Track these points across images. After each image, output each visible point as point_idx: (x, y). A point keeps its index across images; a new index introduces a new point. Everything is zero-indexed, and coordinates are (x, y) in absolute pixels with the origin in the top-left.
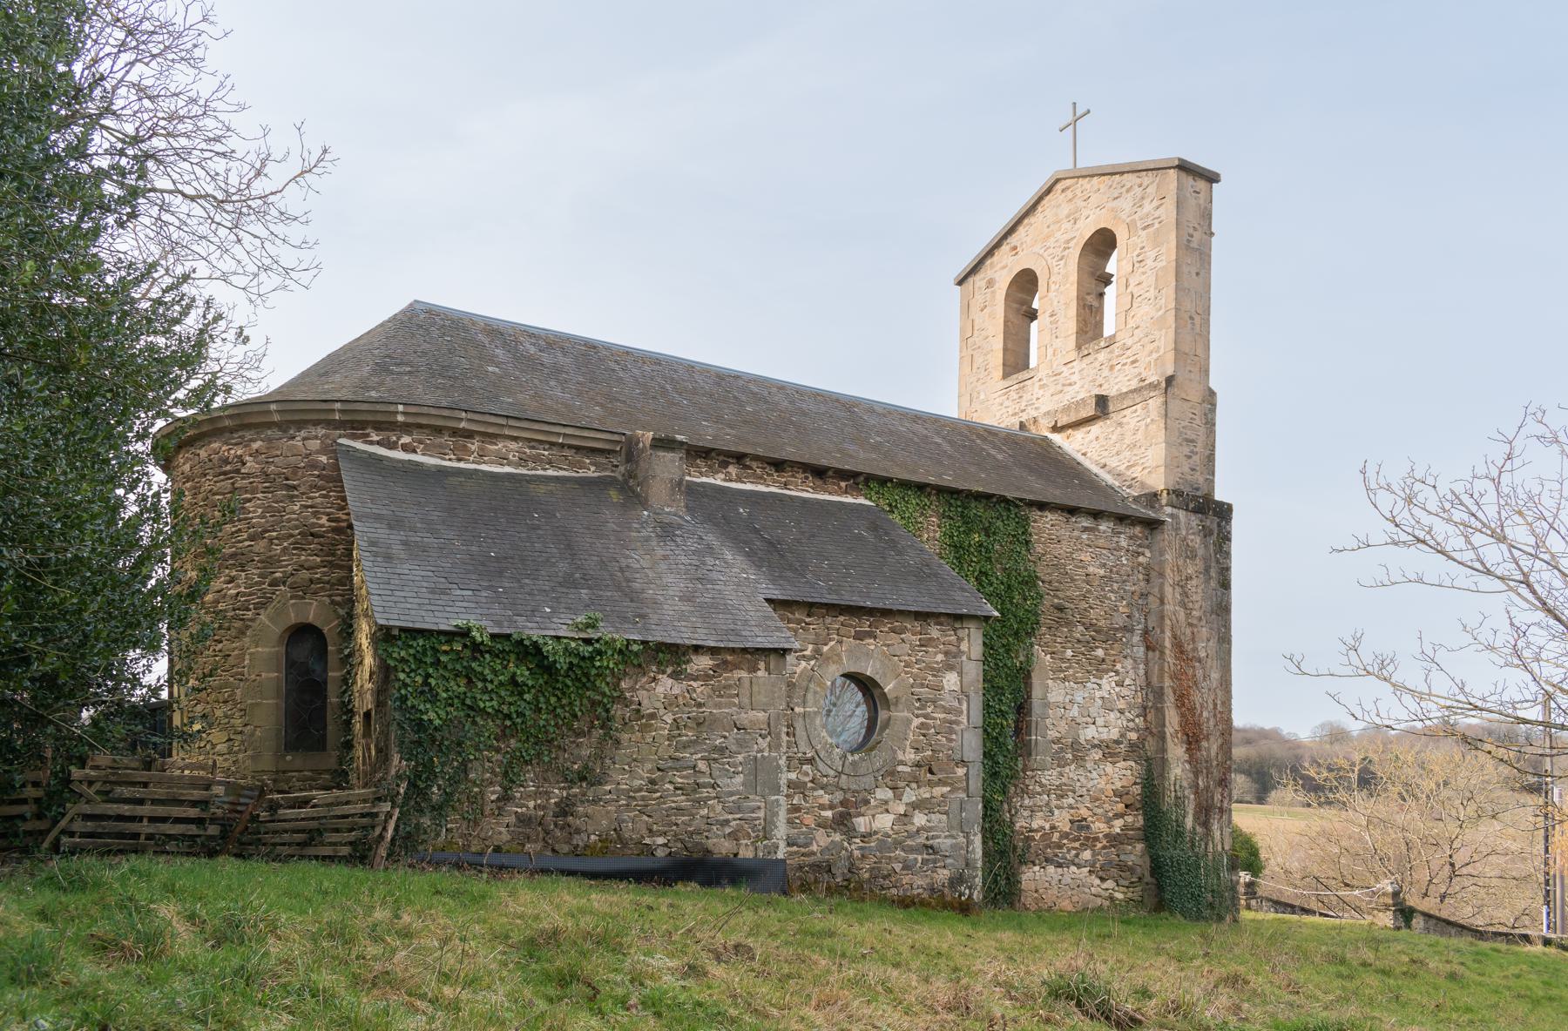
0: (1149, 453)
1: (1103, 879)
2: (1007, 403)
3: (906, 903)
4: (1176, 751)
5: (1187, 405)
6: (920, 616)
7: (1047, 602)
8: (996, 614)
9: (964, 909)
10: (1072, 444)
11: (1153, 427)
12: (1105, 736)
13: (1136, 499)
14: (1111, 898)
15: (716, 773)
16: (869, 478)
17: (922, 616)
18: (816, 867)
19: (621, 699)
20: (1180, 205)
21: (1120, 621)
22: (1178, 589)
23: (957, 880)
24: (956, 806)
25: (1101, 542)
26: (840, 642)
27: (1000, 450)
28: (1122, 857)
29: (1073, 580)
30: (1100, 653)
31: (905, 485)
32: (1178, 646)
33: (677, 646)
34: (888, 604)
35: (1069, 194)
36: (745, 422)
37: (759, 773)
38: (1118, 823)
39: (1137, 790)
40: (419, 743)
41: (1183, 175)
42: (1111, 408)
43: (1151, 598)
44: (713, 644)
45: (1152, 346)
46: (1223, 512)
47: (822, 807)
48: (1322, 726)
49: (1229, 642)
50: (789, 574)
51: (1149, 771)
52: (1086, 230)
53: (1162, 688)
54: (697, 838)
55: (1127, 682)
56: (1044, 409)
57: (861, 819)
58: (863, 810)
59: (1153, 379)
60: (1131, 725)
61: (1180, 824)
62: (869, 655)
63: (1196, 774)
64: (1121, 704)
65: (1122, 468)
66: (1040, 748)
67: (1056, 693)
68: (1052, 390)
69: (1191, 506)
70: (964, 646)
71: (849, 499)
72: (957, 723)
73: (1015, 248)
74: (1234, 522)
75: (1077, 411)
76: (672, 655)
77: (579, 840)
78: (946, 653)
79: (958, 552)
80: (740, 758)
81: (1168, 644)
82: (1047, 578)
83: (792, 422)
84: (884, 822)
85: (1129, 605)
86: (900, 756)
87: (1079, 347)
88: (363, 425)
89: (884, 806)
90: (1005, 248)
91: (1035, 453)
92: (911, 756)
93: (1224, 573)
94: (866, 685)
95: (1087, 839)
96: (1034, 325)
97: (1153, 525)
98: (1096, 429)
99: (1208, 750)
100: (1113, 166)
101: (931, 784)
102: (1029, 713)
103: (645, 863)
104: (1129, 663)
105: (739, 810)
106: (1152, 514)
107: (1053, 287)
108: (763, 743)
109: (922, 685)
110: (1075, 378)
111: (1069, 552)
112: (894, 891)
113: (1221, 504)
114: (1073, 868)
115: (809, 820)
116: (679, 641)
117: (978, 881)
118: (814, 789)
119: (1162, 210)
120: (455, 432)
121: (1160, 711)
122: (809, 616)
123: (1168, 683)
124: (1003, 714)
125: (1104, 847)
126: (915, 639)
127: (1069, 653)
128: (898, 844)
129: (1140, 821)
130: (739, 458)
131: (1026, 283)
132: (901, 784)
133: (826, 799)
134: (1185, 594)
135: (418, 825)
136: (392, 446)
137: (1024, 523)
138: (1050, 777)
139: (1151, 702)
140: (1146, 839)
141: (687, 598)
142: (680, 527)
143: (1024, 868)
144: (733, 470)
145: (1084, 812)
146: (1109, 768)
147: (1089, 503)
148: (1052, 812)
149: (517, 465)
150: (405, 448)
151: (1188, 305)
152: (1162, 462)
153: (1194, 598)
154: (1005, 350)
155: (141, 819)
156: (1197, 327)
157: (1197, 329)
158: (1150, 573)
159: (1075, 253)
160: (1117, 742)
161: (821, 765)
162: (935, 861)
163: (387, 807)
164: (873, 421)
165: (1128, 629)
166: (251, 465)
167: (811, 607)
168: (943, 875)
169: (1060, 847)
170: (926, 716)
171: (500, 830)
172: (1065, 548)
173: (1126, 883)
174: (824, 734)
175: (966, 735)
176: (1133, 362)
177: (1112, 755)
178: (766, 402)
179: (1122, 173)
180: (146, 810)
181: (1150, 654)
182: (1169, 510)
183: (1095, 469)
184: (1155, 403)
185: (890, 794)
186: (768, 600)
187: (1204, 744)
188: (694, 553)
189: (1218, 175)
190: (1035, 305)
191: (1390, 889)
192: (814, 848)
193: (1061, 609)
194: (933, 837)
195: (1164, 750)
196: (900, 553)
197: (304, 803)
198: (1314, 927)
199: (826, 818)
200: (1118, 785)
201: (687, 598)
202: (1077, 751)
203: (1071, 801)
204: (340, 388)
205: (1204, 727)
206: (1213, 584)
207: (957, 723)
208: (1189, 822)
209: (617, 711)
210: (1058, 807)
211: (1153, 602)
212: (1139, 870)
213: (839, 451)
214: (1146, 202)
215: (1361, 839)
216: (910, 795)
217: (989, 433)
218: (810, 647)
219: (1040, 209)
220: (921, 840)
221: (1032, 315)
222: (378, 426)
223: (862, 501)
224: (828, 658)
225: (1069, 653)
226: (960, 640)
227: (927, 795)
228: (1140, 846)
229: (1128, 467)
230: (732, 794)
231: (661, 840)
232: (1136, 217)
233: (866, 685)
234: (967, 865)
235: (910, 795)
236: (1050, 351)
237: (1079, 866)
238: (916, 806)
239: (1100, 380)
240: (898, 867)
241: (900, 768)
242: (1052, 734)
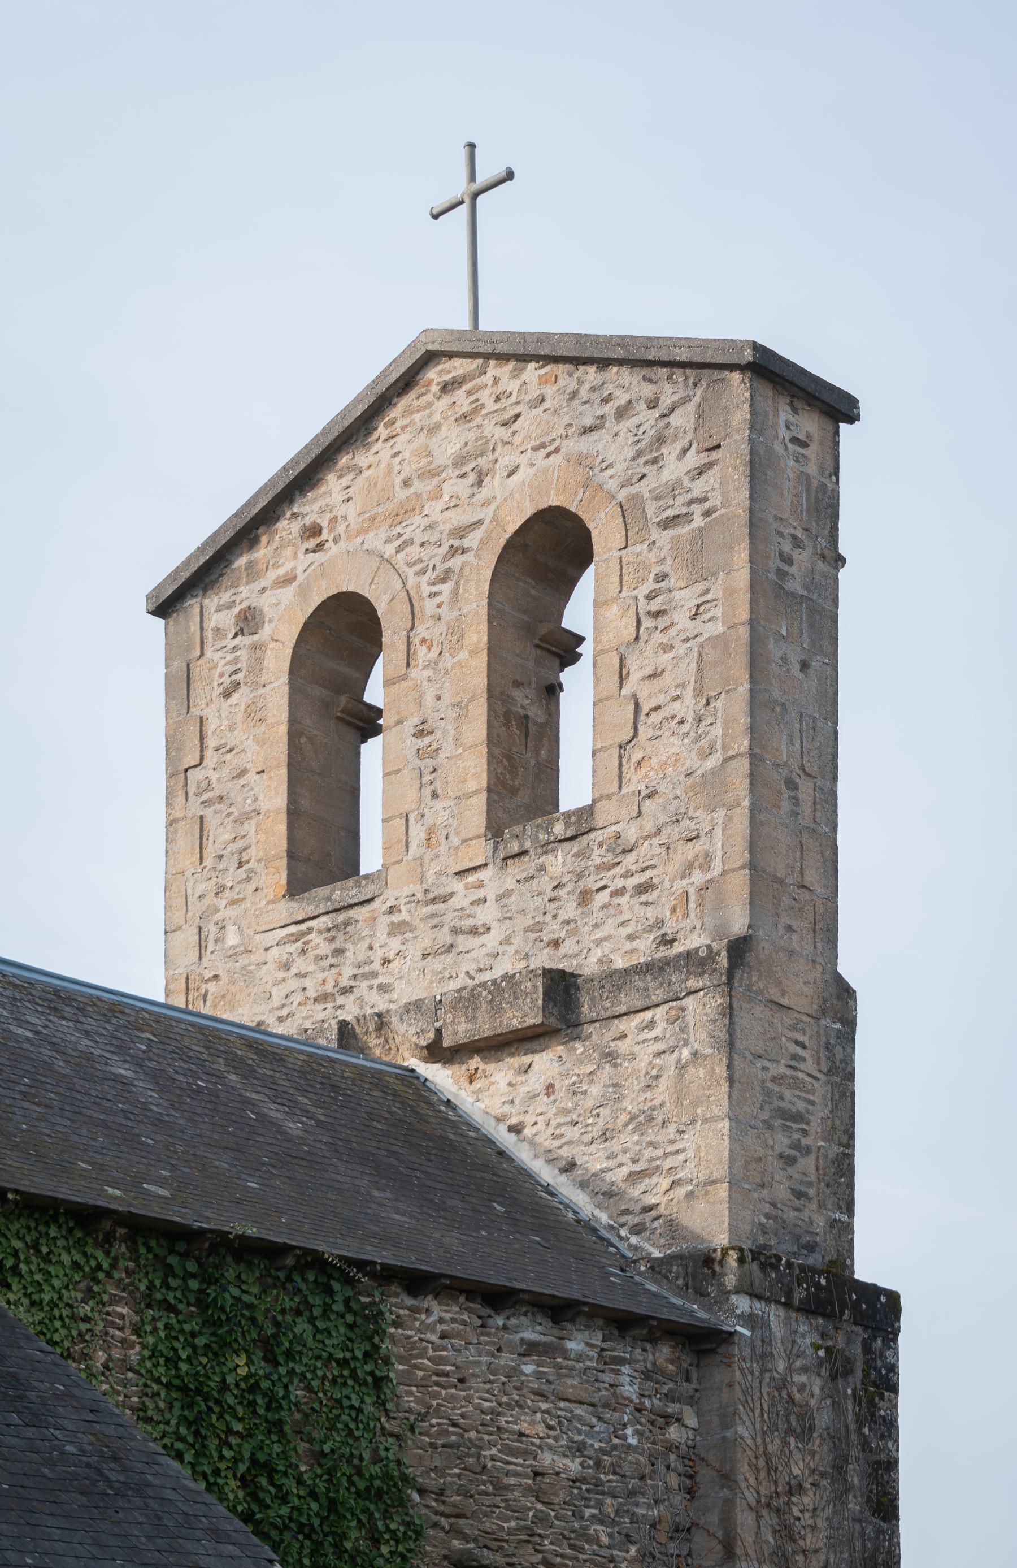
0: (688, 1141)
2: (300, 964)
5: (781, 1022)
10: (485, 1097)
11: (698, 1073)
13: (657, 1267)
22: (769, 1519)
25: (571, 1385)
27: (293, 1108)
29: (500, 1488)
41: (766, 391)
43: (699, 1539)
46: (878, 1313)
52: (511, 502)
56: (405, 992)
59: (695, 941)
65: (618, 1176)
68: (425, 939)
69: (799, 1294)
73: (314, 530)
74: (904, 1341)
75: (496, 1010)
79: (192, 1403)
82: (432, 1482)
87: (495, 830)
90: (287, 527)
91: (364, 1108)
96: (372, 752)
97: (703, 1343)
98: (545, 1063)
100: (580, 339)
106: (699, 1312)
107: (422, 654)
110: (487, 914)
113: (872, 1292)
119: (711, 478)
131: (344, 633)
134: (786, 1532)
137: (369, 1326)
147: (542, 1272)
151: (783, 749)
152: (721, 1171)
153: (809, 1541)
156: (807, 809)
172: (479, 1398)
176: (643, 889)
179: (604, 363)
182: (742, 1304)
183: (546, 1174)
184: (702, 1008)
189: (852, 402)
190: (374, 694)
206: (854, 1505)
214: (670, 452)
217: (256, 1053)
221: (367, 723)
229: (634, 1177)
232: (644, 488)
239: (553, 929)
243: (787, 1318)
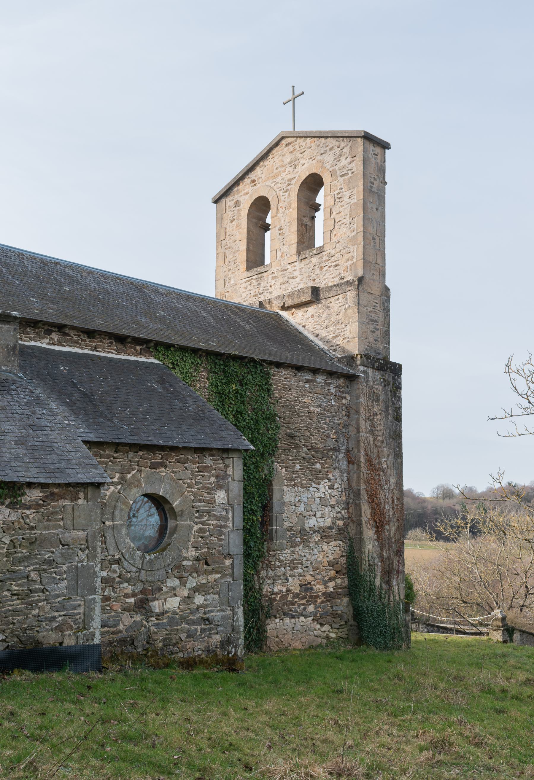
0: (348, 328)
1: (322, 625)
2: (249, 288)
3: (189, 664)
4: (369, 533)
7: (282, 431)
8: (252, 447)
9: (231, 665)
10: (296, 319)
11: (350, 311)
12: (322, 524)
13: (340, 360)
14: (328, 638)
15: (45, 581)
16: (158, 344)
17: (200, 450)
18: (122, 642)
20: (365, 162)
21: (331, 444)
22: (368, 422)
23: (226, 642)
24: (225, 588)
25: (318, 390)
26: (140, 471)
28: (334, 608)
29: (299, 416)
30: (318, 466)
31: (183, 349)
32: (369, 461)
33: (14, 483)
34: (174, 442)
35: (291, 148)
36: (63, 299)
37: (80, 580)
38: (331, 584)
39: (343, 560)
41: (367, 142)
42: (322, 296)
43: (351, 428)
44: (42, 481)
45: (348, 256)
48: (438, 488)
49: (401, 458)
50: (101, 420)
51: (351, 547)
52: (303, 173)
53: (359, 490)
54: (30, 633)
55: (336, 486)
56: (276, 293)
57: (156, 603)
58: (157, 595)
59: (349, 278)
60: (339, 515)
61: (372, 583)
62: (161, 480)
63: (382, 548)
64: (332, 502)
66: (279, 534)
67: (289, 496)
68: (281, 280)
69: (376, 365)
70: (230, 471)
71: (143, 359)
72: (225, 527)
73: (254, 181)
74: (403, 376)
75: (299, 297)
78: (217, 477)
79: (221, 397)
80: (64, 567)
81: (362, 459)
82: (282, 415)
83: (99, 300)
84: (173, 603)
85: (337, 433)
86: (185, 554)
87: (299, 253)
90: (247, 180)
91: (267, 323)
92: (192, 553)
93: (398, 410)
94: (159, 502)
95: (311, 597)
96: (268, 235)
97: (351, 378)
98: (311, 310)
99: (389, 531)
100: (320, 132)
101: (207, 573)
102: (271, 510)
104: (337, 473)
105: (64, 608)
107: (280, 210)
108: (83, 555)
109: (200, 501)
110: (296, 273)
111: (299, 398)
112: (181, 655)
113: (394, 364)
114: (302, 618)
115: (117, 606)
116: (15, 480)
117: (241, 641)
118: (120, 583)
119: (353, 164)
121: (358, 506)
122: (116, 452)
123: (363, 486)
124: (253, 512)
125: (323, 602)
126: (195, 467)
127: (298, 467)
128: (184, 619)
129: (346, 582)
130: (60, 328)
131: (261, 205)
132: (186, 574)
133: (129, 589)
134: (373, 426)
137: (266, 376)
138: (285, 555)
139: (351, 501)
140: (350, 594)
141: (22, 442)
142: (14, 382)
143: (269, 621)
144: (55, 336)
145: (309, 578)
146: (325, 547)
148: (287, 579)
151: (372, 230)
152: (356, 335)
153: (379, 428)
154: (248, 250)
156: (377, 244)
157: (377, 247)
158: (351, 411)
159: (295, 188)
160: (330, 528)
161: (126, 564)
162: (210, 630)
164: (158, 299)
165: (336, 450)
167: (117, 446)
168: (216, 639)
169: (293, 604)
170: (203, 523)
172: (294, 394)
173: (337, 626)
174: (128, 540)
175: (231, 536)
176: (336, 265)
177: (327, 537)
178: (79, 283)
179: (326, 137)
181: (351, 466)
182: (362, 368)
183: (311, 337)
184: (351, 295)
185: (177, 582)
186: (85, 442)
187: (387, 527)
188: (26, 403)
189: (389, 144)
190: (268, 220)
191: (500, 616)
192: (121, 627)
193: (291, 436)
194: (209, 612)
195: (361, 533)
196: (182, 401)
198: (457, 645)
199: (130, 604)
200: (331, 557)
201: (22, 442)
202: (303, 536)
203: (300, 571)
205: (387, 515)
206: (390, 418)
207: (225, 527)
210: (291, 576)
211: (352, 431)
212: (345, 616)
213: (135, 322)
214: (343, 158)
215: (471, 572)
218: (117, 475)
219: (271, 156)
220: (200, 615)
221: (266, 228)
223: (152, 360)
224: (131, 484)
225: (298, 467)
226: (227, 466)
227: (204, 581)
228: (346, 600)
229: (334, 337)
230: (58, 596)
232: (336, 167)
233: (159, 502)
234: (233, 630)
235: (192, 582)
236: (279, 254)
237: (306, 617)
238: (196, 590)
239: (313, 276)
240: (183, 636)
241: (184, 563)
242: (287, 524)
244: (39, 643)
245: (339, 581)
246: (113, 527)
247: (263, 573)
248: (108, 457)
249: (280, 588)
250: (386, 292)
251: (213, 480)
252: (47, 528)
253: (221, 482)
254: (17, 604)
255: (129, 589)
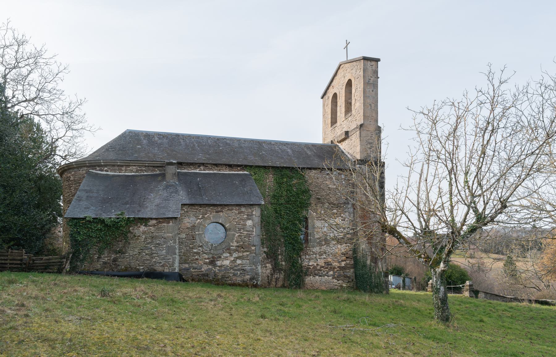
1: (338, 281)
5: (369, 133)
6: (237, 205)
14: (341, 286)
16: (246, 166)
18: (204, 275)
19: (130, 232)
30: (335, 211)
34: (225, 203)
39: (351, 253)
40: (76, 245)
41: (366, 61)
47: (205, 259)
62: (220, 217)
67: (318, 224)
70: (254, 213)
71: (241, 172)
72: (252, 234)
76: (144, 221)
77: (119, 268)
78: (247, 215)
84: (227, 263)
86: (232, 244)
88: (95, 166)
89: (226, 258)
90: (331, 87)
92: (235, 244)
95: (331, 268)
98: (347, 141)
101: (243, 252)
103: (137, 273)
104: (347, 214)
111: (328, 183)
120: (118, 166)
126: (237, 212)
128: (231, 268)
129: (352, 262)
131: (335, 96)
133: (207, 257)
135: (77, 265)
136: (102, 171)
143: (307, 277)
145: (329, 260)
146: (339, 246)
149: (135, 172)
150: (106, 171)
155: (7, 264)
161: (204, 247)
163: (65, 260)
166: (72, 178)
167: (200, 205)
168: (248, 277)
169: (321, 270)
170: (241, 233)
171: (98, 266)
172: (320, 180)
180: (8, 261)
182: (358, 166)
185: (228, 255)
192: (203, 270)
197: (42, 259)
203: (325, 256)
204: (112, 156)
208: (368, 262)
209: (129, 235)
210: (320, 258)
216: (235, 255)
222: (99, 166)
231: (142, 268)
235: (235, 255)
237: (328, 276)
238: (237, 258)
240: (231, 275)
243: (343, 166)
244: (155, 270)
245: (348, 262)
246: (198, 234)
247: (303, 257)
248: (197, 209)
249: (313, 263)
250: (379, 130)
251: (245, 216)
252: (158, 233)
253: (249, 217)
254: (148, 257)
255: (207, 257)
